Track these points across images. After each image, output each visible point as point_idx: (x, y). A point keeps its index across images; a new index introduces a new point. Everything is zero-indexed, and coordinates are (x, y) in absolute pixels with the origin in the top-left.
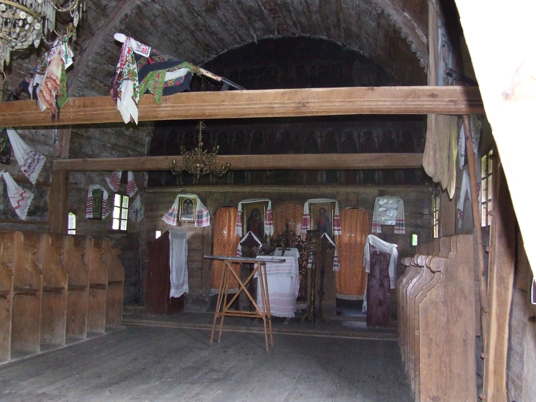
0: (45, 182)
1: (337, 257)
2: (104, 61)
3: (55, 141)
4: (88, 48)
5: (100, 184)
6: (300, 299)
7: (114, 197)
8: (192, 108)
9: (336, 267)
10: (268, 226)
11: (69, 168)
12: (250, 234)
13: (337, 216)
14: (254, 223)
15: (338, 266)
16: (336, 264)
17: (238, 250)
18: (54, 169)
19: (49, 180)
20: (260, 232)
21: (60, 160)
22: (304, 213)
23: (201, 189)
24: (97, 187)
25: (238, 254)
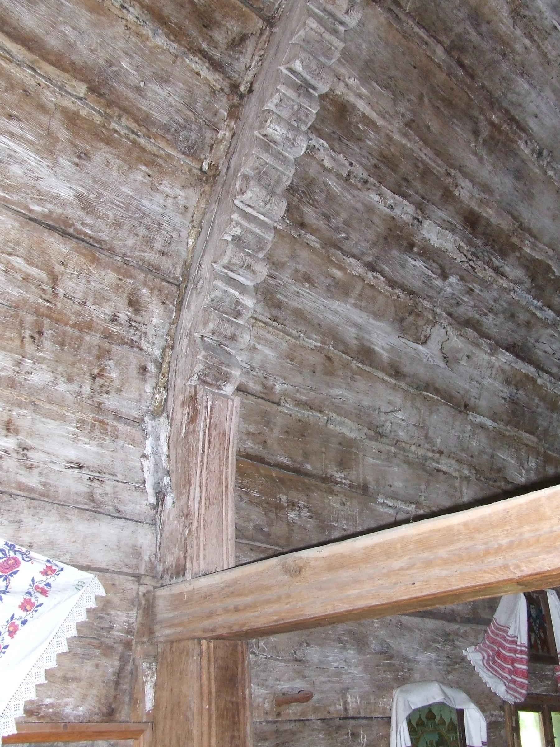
0: (110, 714)
2: (360, 171)
3: (160, 495)
4: (261, 78)
5: (444, 682)
7: (516, 729)
11: (224, 622)
18: (163, 633)
19: (135, 700)
21: (181, 587)
24: (428, 695)
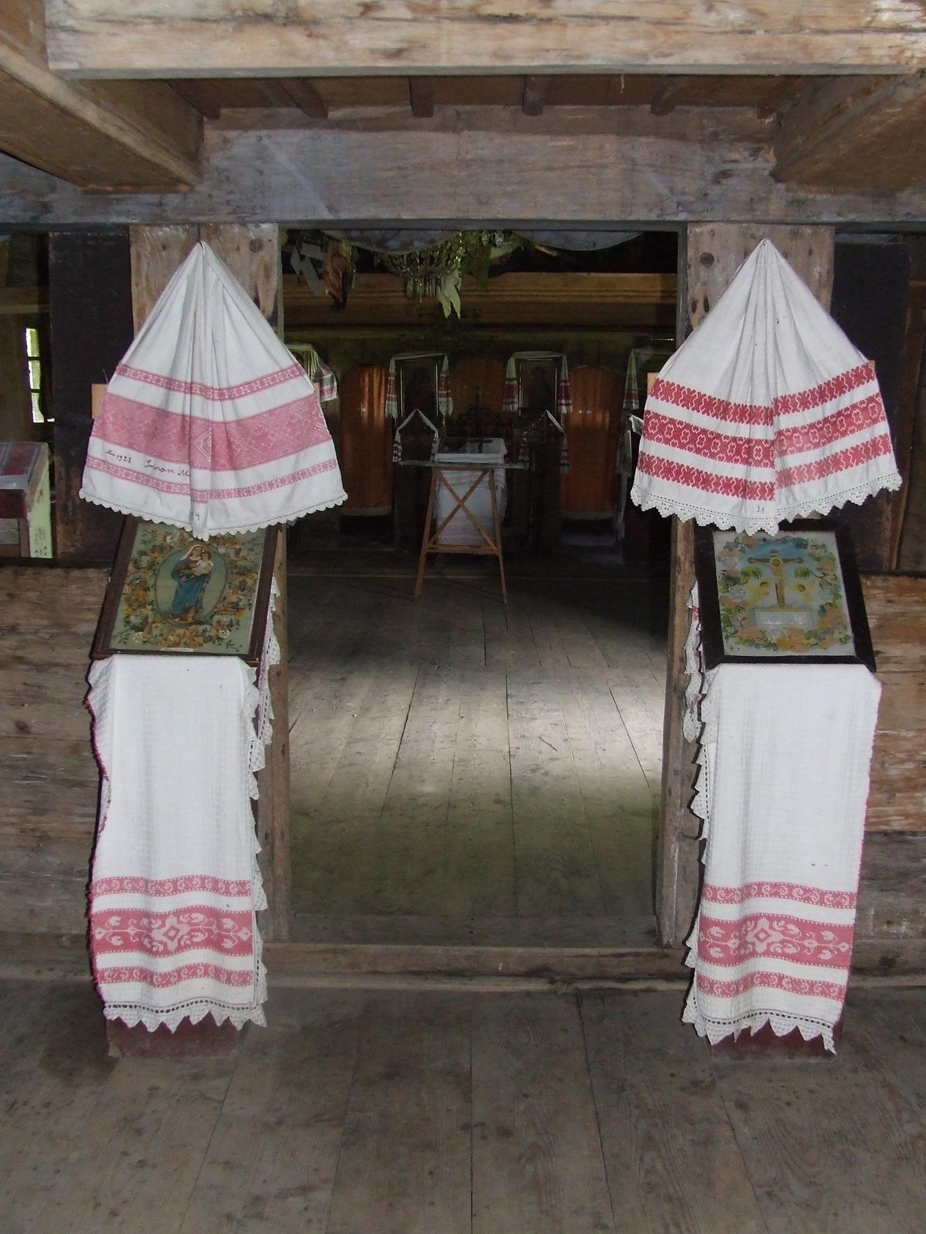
1: (566, 451)
6: (507, 522)
8: (813, 456)
9: (566, 468)
10: (444, 399)
12: (417, 414)
13: (565, 382)
14: (418, 395)
15: (568, 465)
16: (566, 462)
17: (397, 442)
20: (430, 408)
22: (508, 376)
23: (318, 334)
25: (397, 449)
